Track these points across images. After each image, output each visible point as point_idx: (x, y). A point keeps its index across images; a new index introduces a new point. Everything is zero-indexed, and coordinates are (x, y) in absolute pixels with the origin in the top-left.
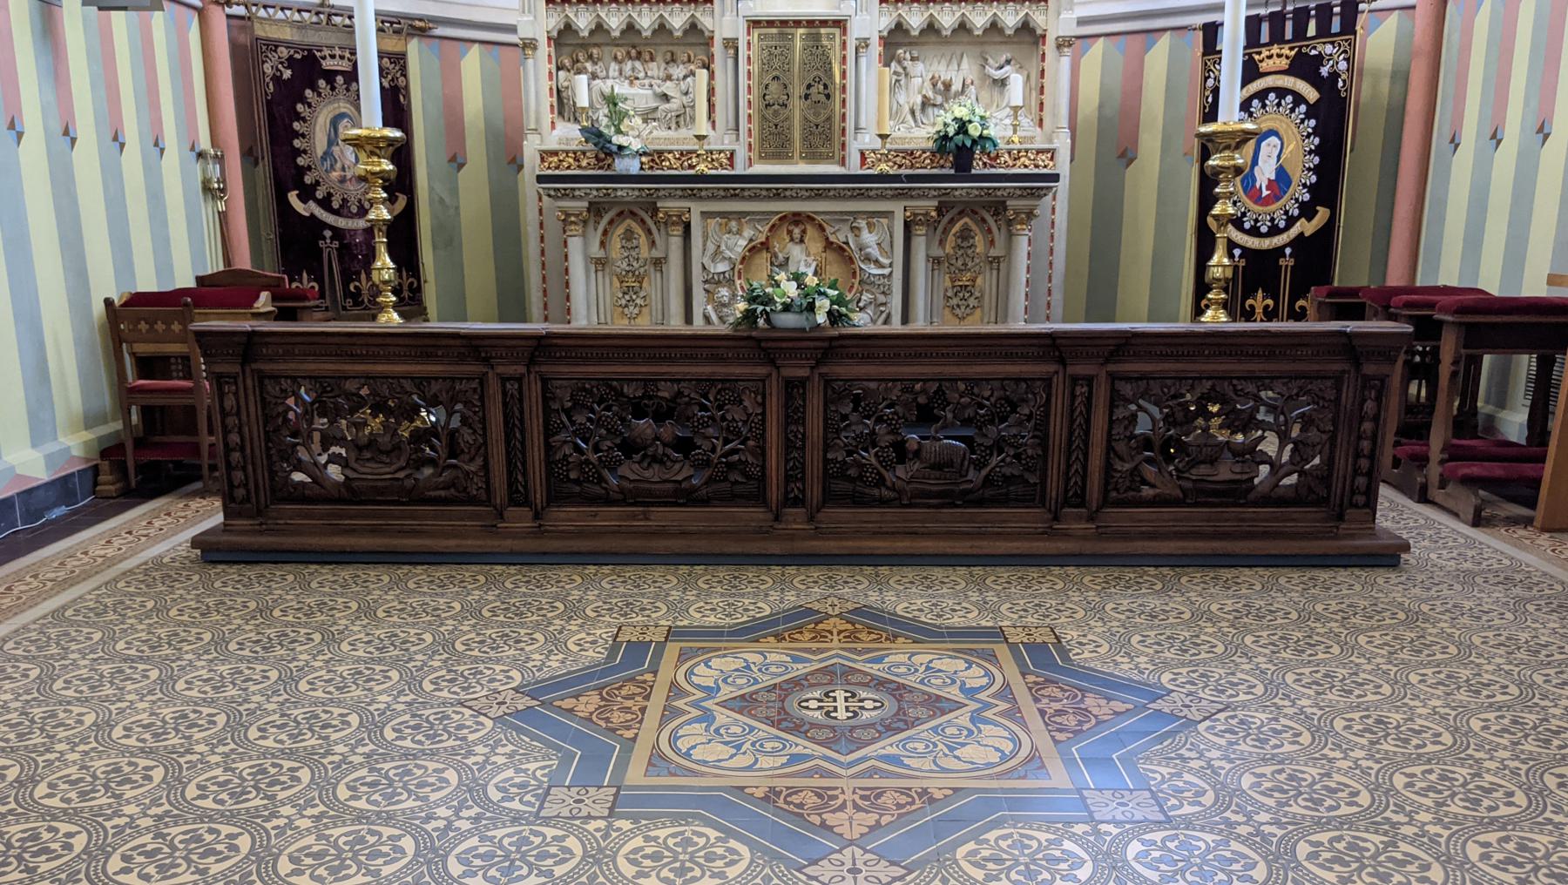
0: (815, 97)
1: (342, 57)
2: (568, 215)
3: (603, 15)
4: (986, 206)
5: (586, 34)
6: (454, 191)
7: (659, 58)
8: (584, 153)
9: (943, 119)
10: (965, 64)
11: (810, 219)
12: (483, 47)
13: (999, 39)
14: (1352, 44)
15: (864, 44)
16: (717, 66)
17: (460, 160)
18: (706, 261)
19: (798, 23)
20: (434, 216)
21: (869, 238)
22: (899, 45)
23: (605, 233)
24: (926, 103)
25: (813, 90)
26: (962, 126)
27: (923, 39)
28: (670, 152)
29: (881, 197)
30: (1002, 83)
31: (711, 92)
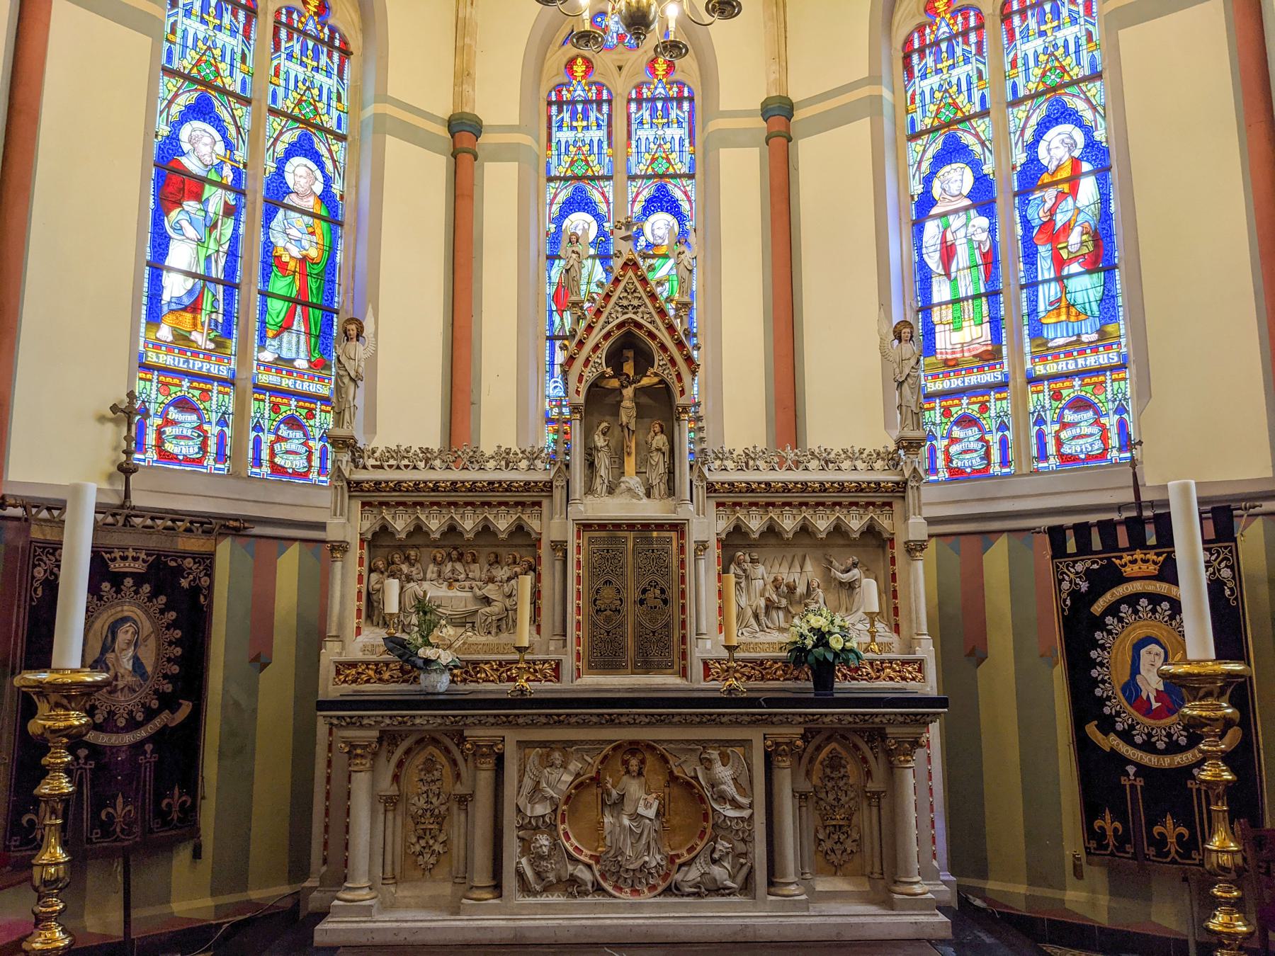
0: (651, 602)
1: (135, 559)
2: (353, 746)
3: (423, 517)
4: (860, 732)
5: (403, 536)
6: (253, 691)
7: (482, 560)
8: (387, 664)
9: (801, 626)
10: (809, 566)
11: (650, 747)
12: (304, 544)
13: (842, 542)
14: (1234, 552)
15: (702, 546)
16: (544, 569)
17: (263, 660)
18: (522, 802)
19: (631, 527)
20: (225, 720)
21: (723, 773)
22: (738, 547)
23: (400, 764)
24: (770, 606)
25: (650, 595)
26: (822, 637)
27: (763, 542)
28: (487, 662)
29: (736, 723)
30: (851, 586)
31: (536, 595)
